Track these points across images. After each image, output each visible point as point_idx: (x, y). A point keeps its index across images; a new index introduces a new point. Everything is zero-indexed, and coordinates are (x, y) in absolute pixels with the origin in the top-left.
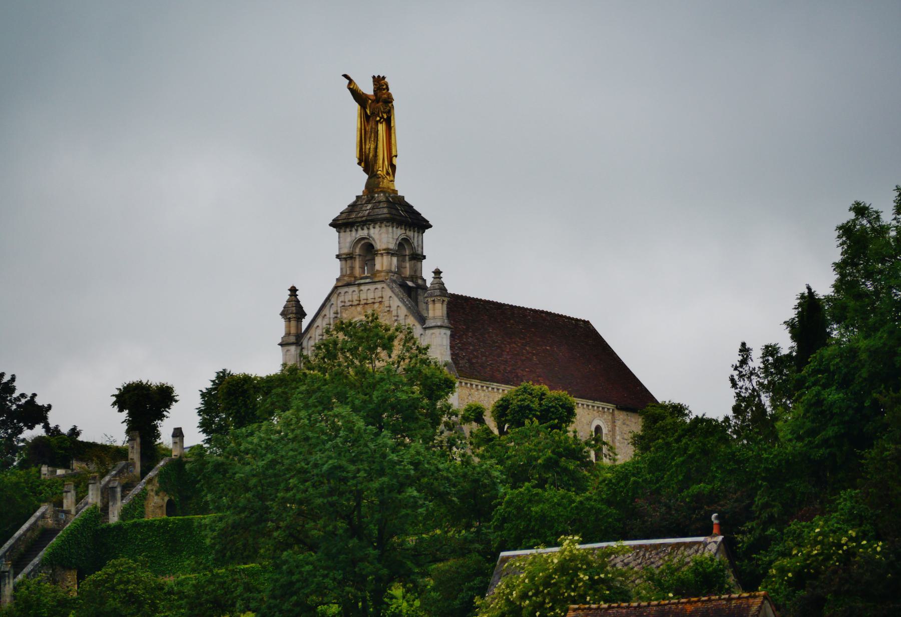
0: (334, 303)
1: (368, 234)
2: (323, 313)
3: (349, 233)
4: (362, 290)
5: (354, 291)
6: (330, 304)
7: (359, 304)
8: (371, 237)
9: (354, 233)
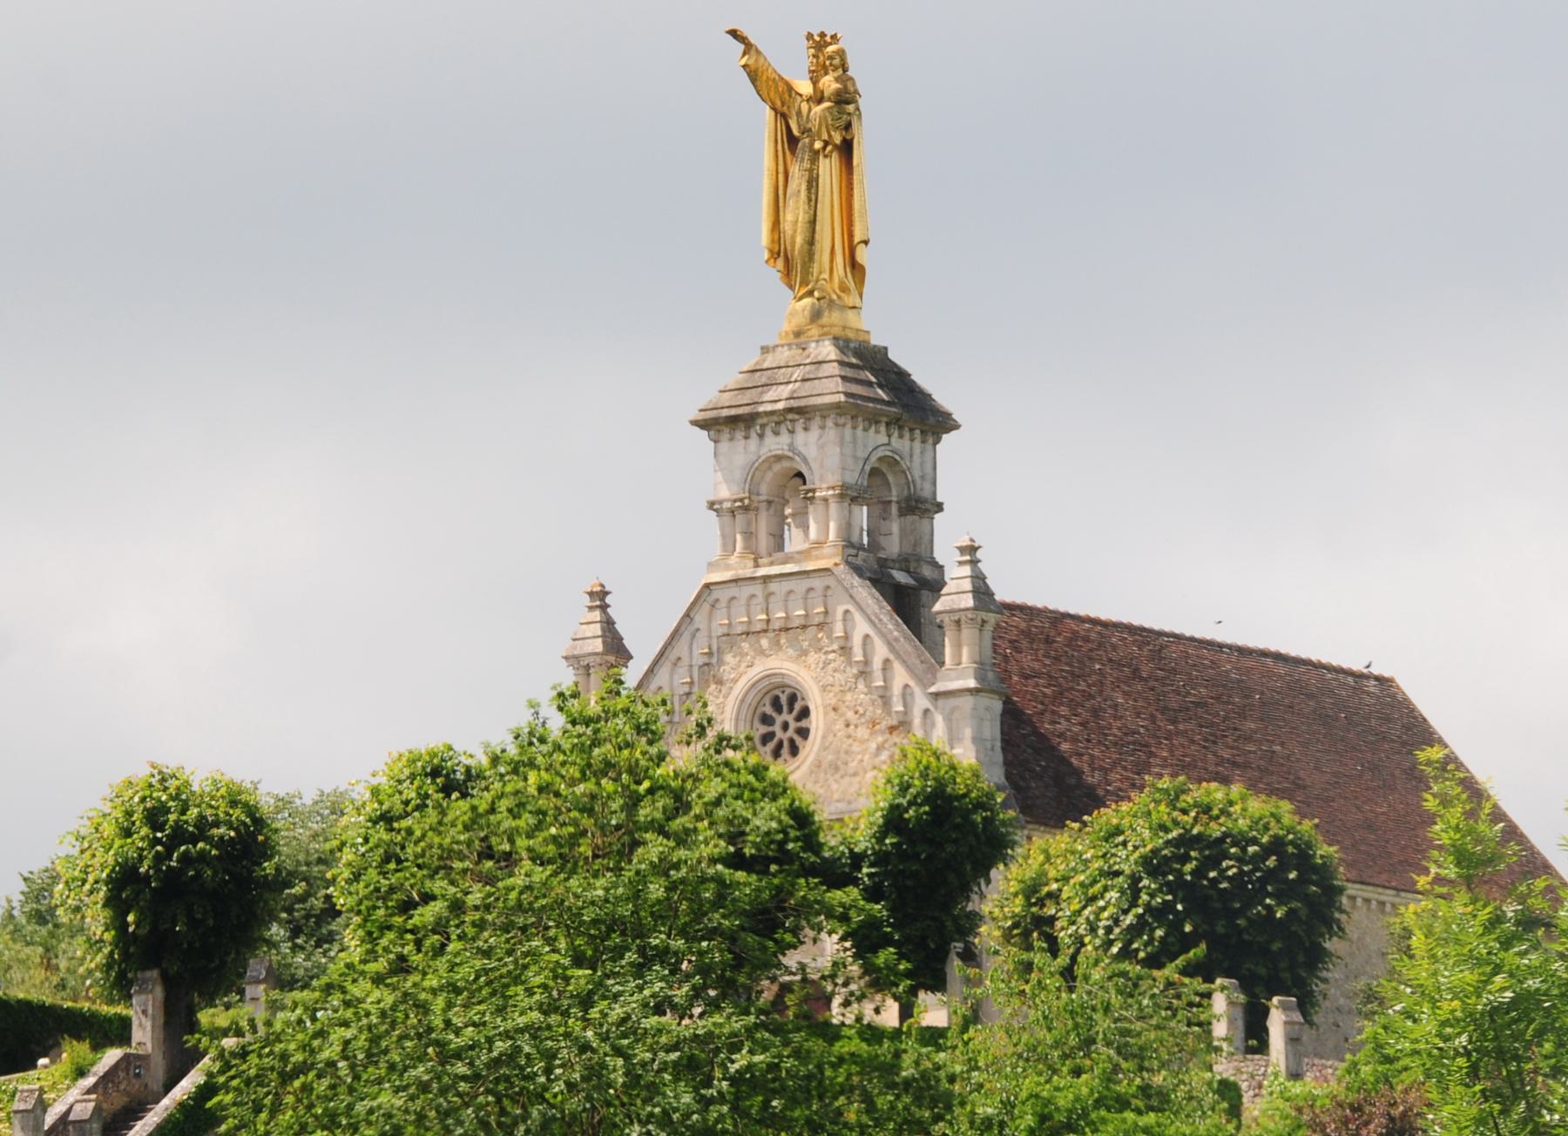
0: (701, 627)
1: (792, 447)
2: (673, 654)
3: (743, 442)
4: (772, 593)
5: (753, 596)
6: (692, 629)
7: (765, 631)
8: (799, 454)
9: (753, 442)
